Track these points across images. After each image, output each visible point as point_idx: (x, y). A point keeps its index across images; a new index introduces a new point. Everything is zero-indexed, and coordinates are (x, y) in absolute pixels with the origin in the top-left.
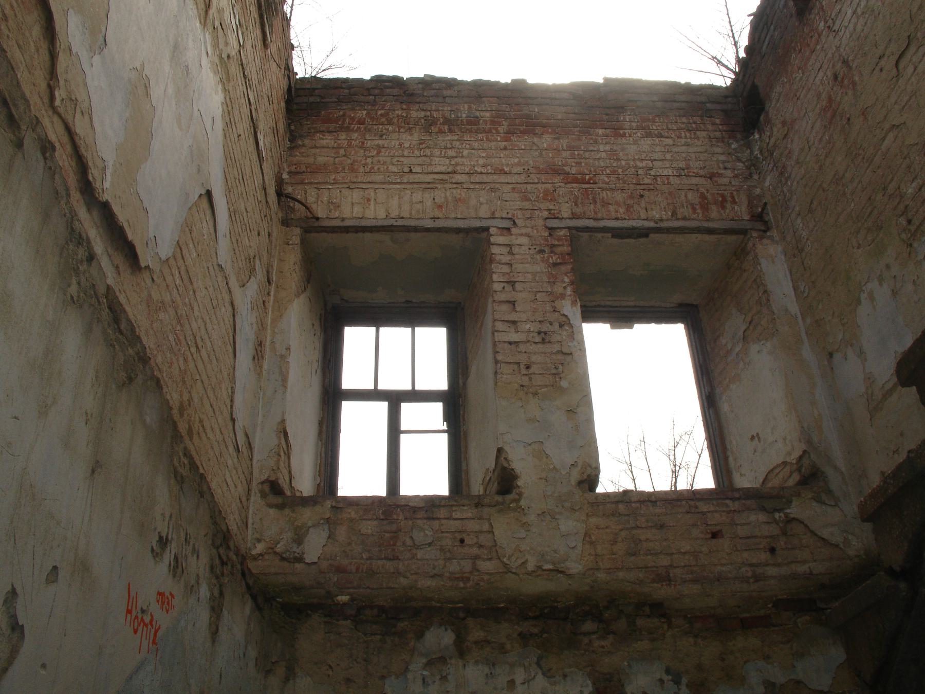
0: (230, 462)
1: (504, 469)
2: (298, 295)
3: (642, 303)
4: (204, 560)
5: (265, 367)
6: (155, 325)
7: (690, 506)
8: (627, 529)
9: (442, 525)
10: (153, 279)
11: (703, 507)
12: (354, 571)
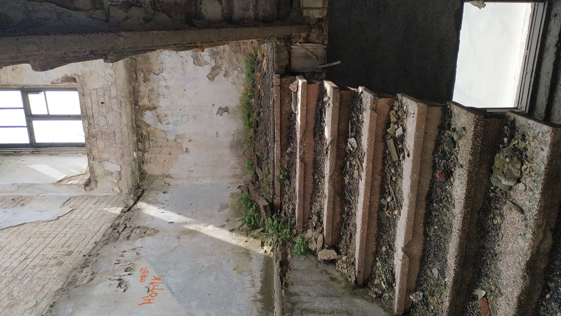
0: (79, 216)
1: (62, 81)
9: (95, 112)
12: (122, 150)
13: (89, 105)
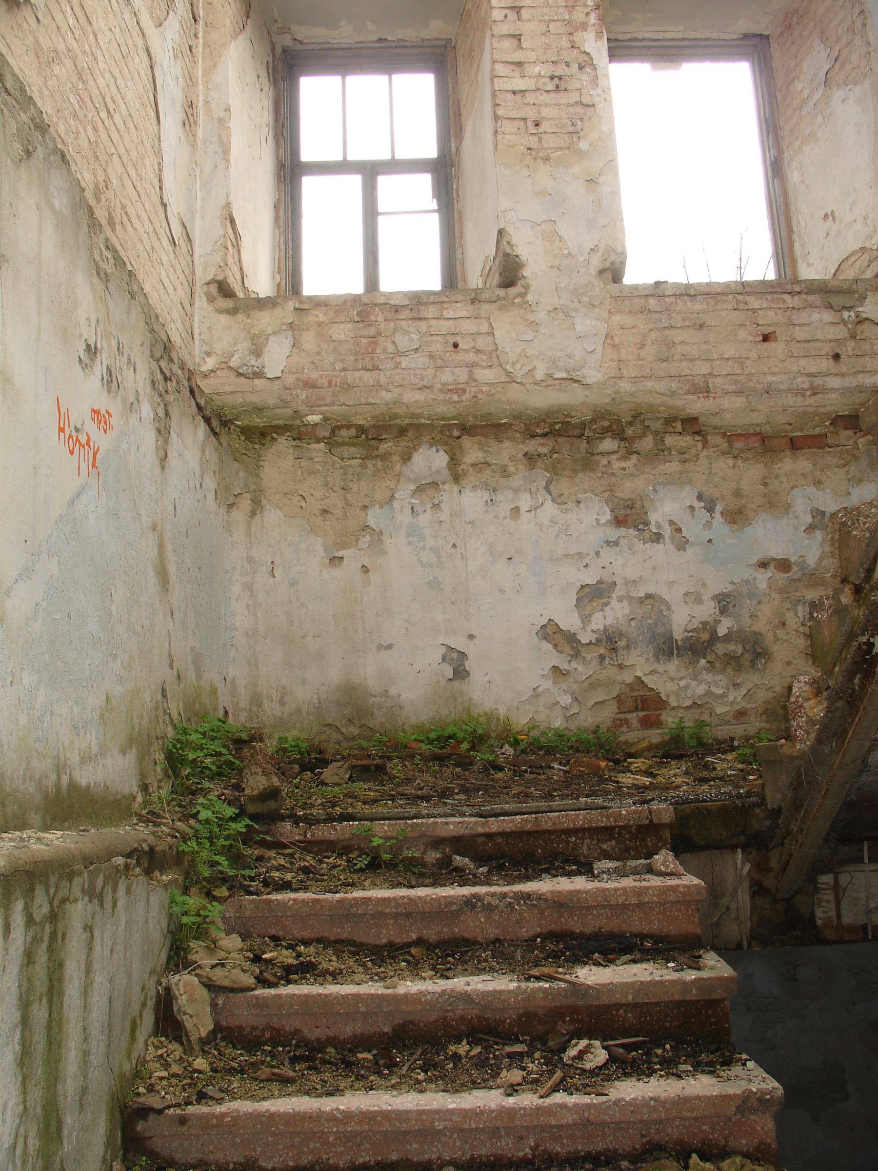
0: (165, 259)
1: (507, 255)
2: (235, 36)
3: (693, 35)
4: (143, 373)
5: (200, 135)
6: (50, 83)
7: (738, 302)
8: (658, 329)
10: (37, 19)
11: (754, 302)
13: (451, 312)
